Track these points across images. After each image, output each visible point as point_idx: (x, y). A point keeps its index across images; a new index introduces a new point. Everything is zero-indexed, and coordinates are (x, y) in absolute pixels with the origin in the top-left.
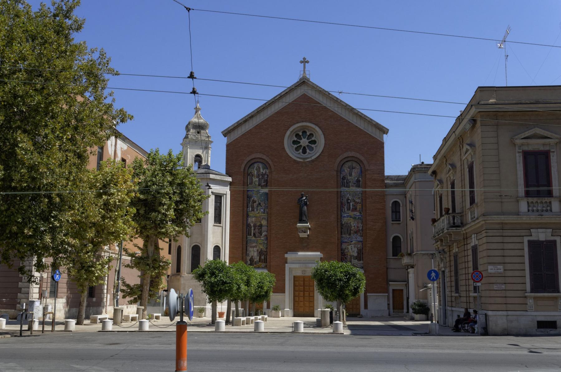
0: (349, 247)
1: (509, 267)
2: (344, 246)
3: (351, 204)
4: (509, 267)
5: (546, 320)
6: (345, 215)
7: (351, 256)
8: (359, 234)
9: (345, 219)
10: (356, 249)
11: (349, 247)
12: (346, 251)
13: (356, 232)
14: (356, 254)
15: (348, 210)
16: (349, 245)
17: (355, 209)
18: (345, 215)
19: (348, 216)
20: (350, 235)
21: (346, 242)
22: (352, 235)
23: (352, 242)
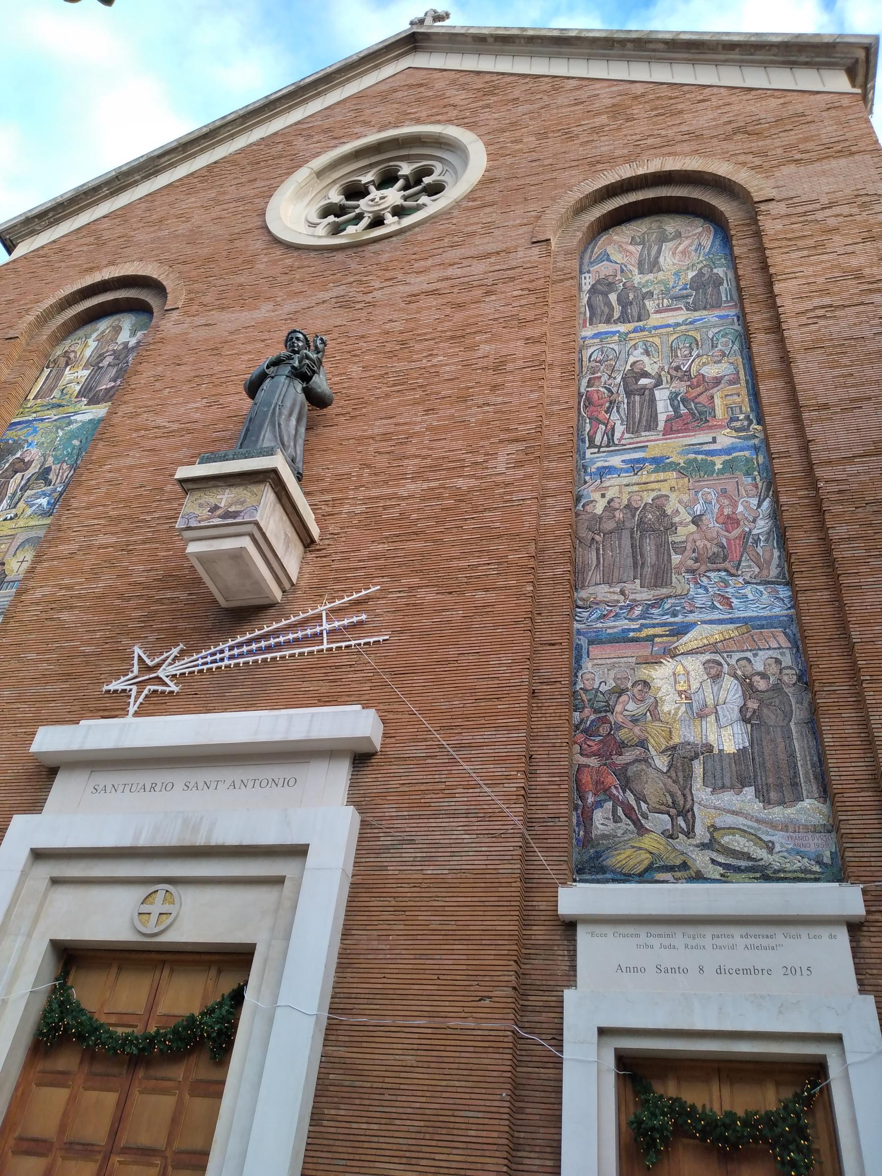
0: (661, 676)
1: (498, 1097)
2: (599, 671)
3: (662, 396)
4: (498, 1097)
5: (813, 1053)
6: (616, 461)
7: (683, 758)
8: (749, 569)
9: (612, 481)
10: (730, 692)
11: (661, 676)
12: (628, 707)
13: (720, 559)
14: (730, 739)
15: (633, 428)
16: (654, 661)
17: (692, 415)
18: (616, 461)
19: (635, 466)
20: (661, 577)
21: (622, 638)
22: (680, 582)
23: (681, 630)
